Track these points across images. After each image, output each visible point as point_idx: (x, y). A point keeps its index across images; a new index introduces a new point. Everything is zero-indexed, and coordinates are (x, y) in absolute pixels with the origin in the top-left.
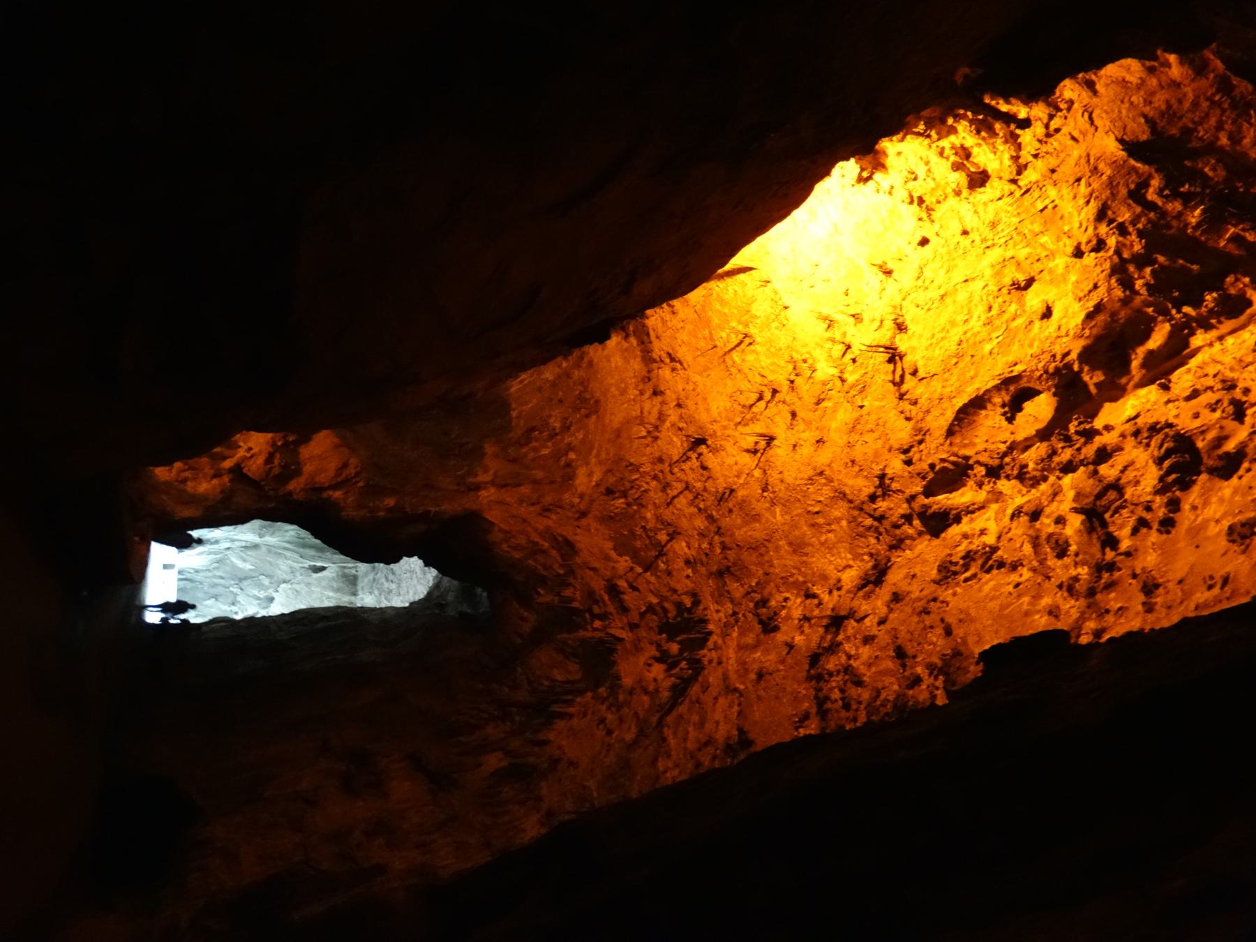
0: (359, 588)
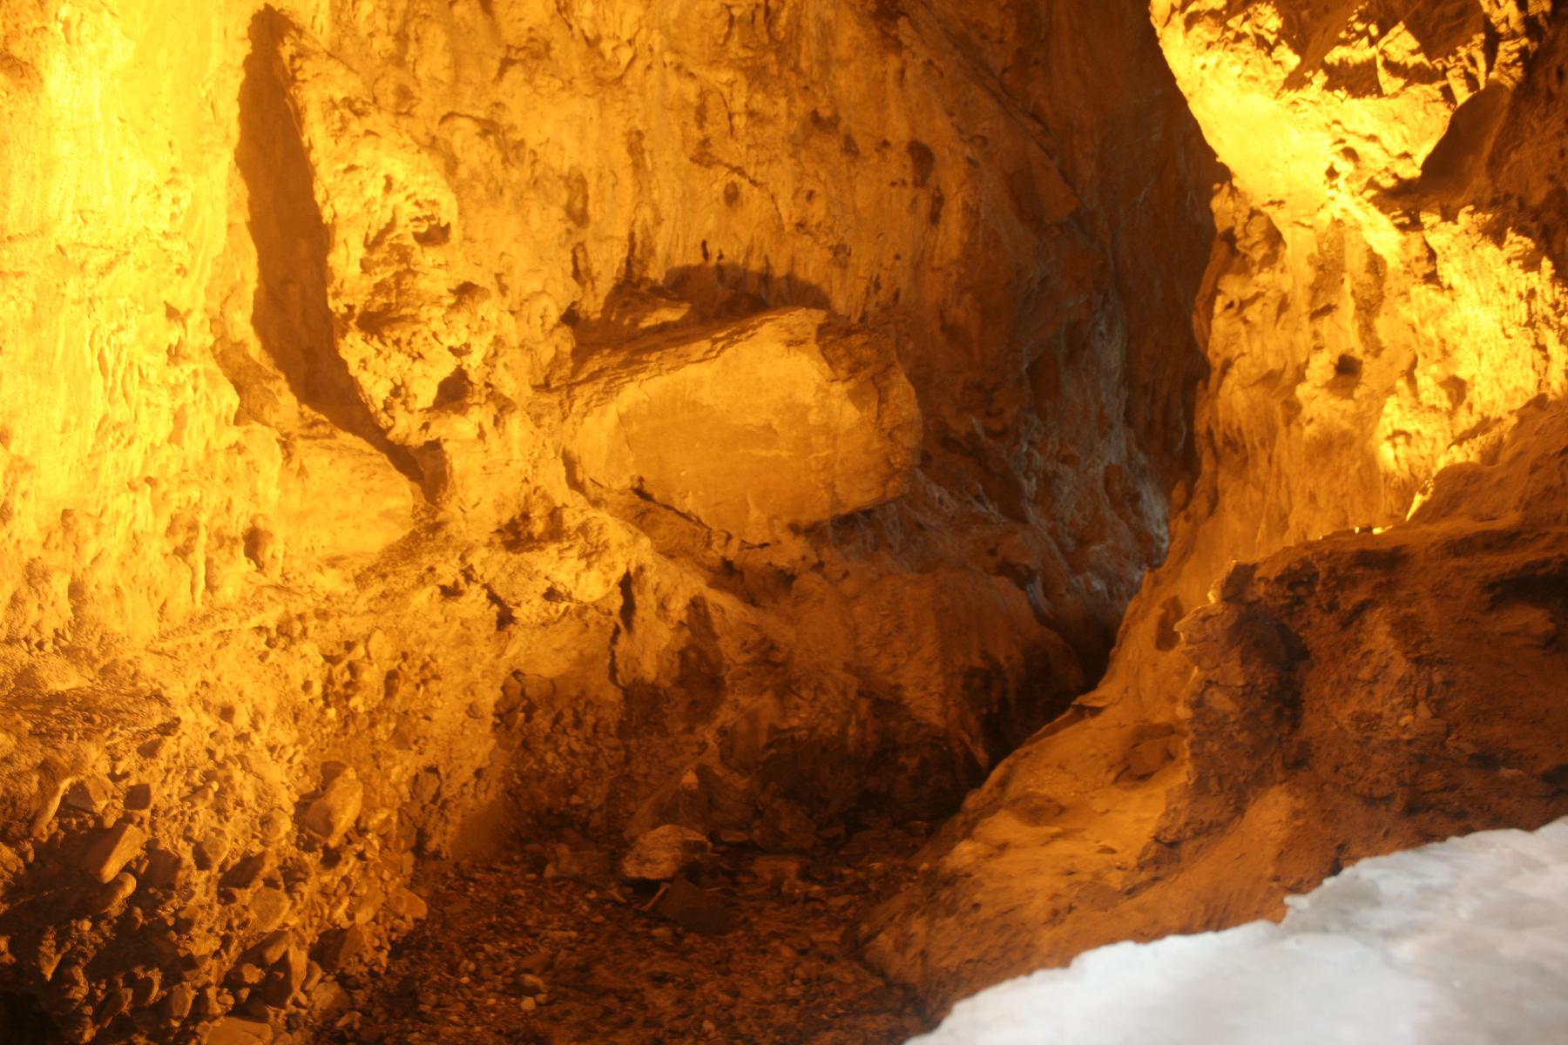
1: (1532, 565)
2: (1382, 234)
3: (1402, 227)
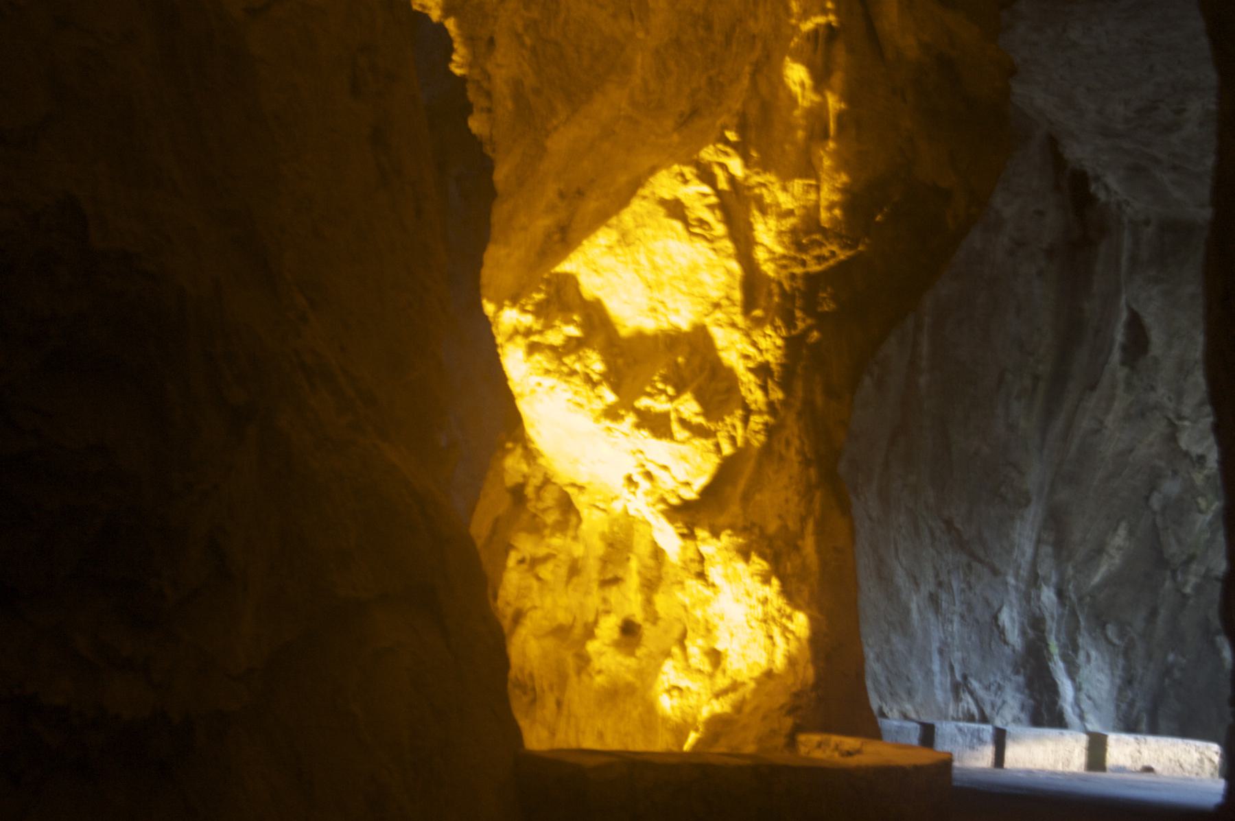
1: (758, 174)
2: (668, 537)
3: (683, 536)
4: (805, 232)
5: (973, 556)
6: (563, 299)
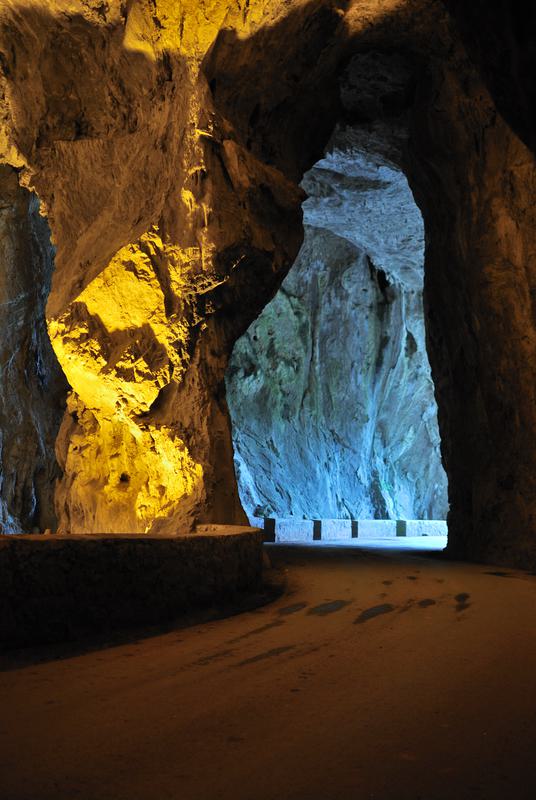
0: (43, 100)
2: (135, 430)
3: (142, 429)
4: (194, 275)
5: (344, 445)
6: (79, 314)
